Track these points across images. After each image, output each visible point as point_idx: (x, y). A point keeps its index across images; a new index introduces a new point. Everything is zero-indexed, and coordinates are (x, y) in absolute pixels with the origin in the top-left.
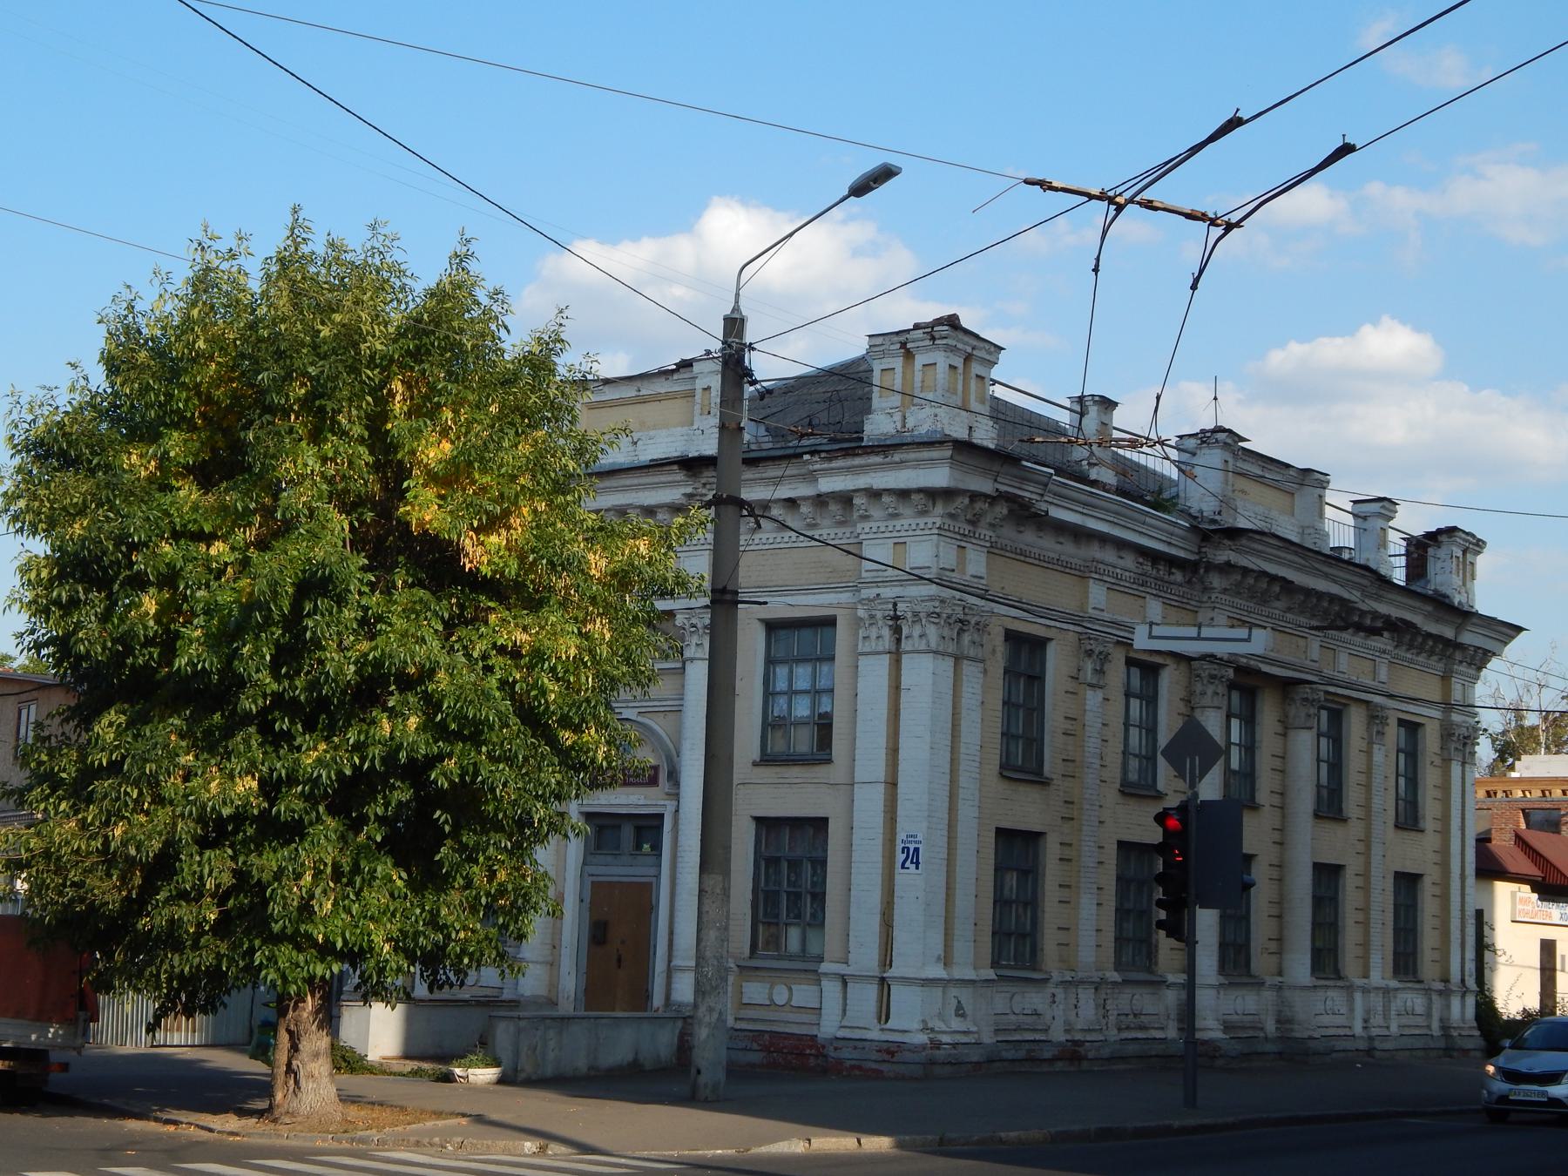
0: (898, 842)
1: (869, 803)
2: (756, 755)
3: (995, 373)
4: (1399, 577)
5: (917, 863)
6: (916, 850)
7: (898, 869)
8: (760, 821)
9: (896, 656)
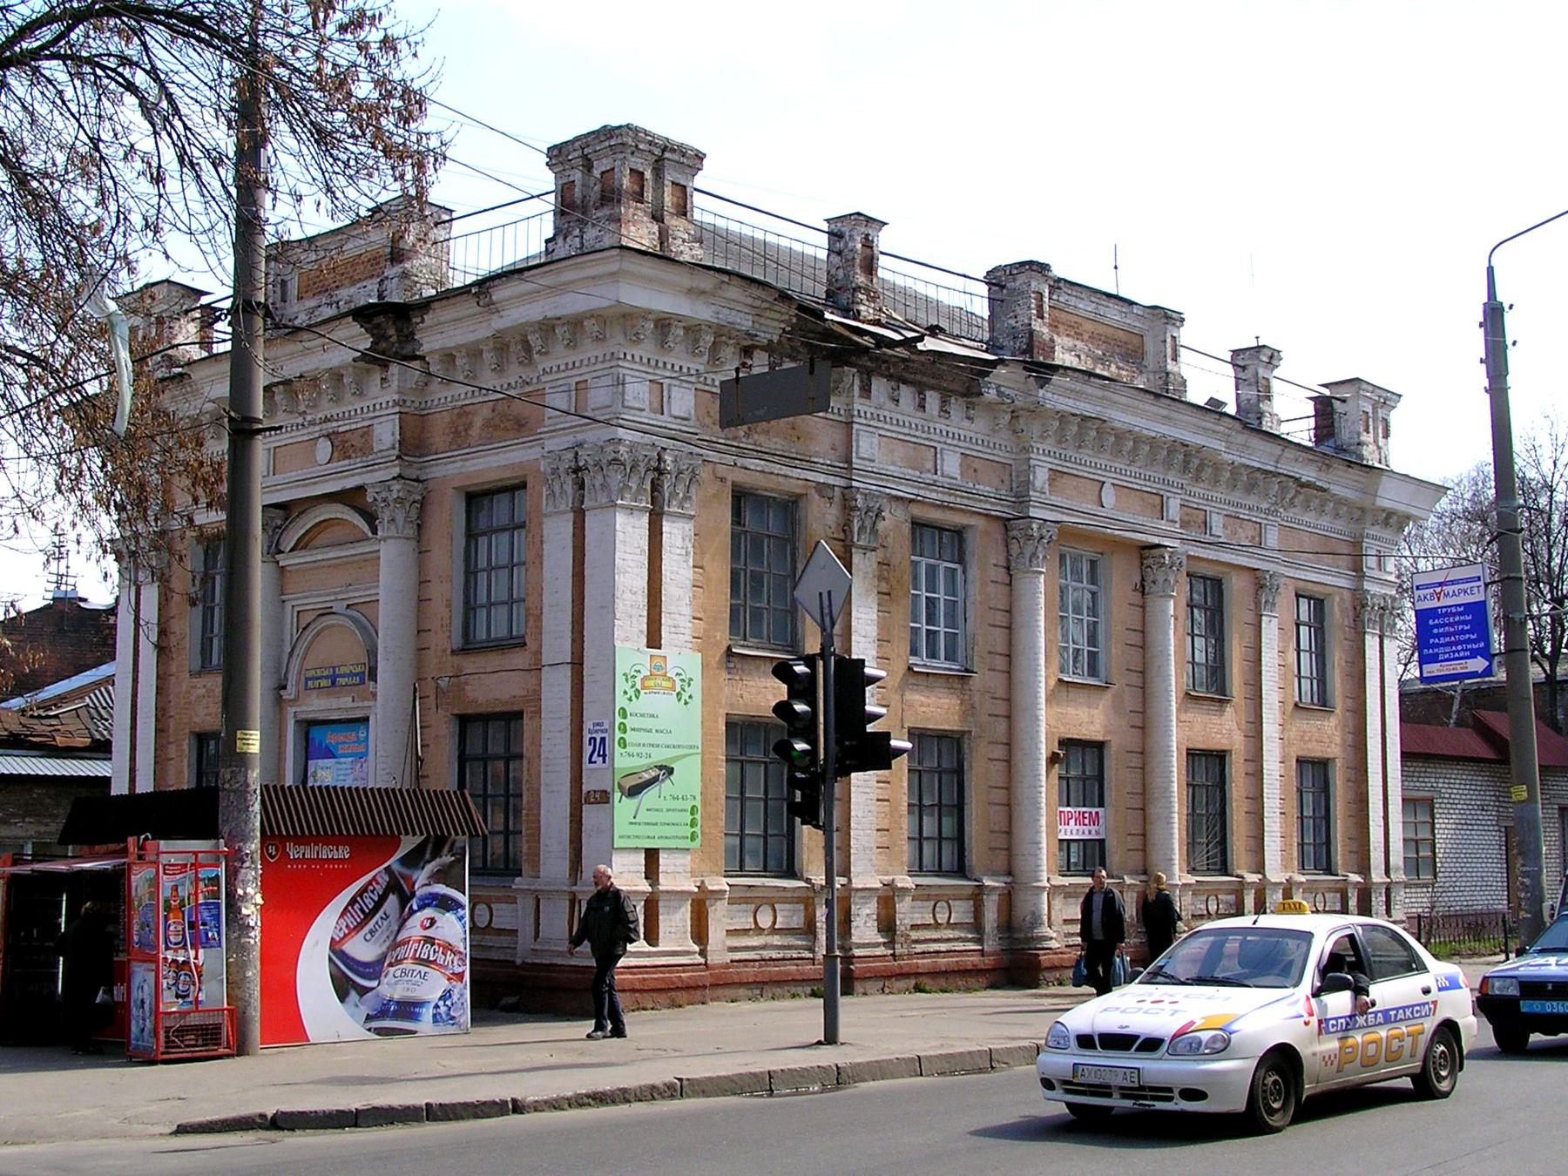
0: (585, 732)
1: (556, 690)
2: (457, 641)
4: (1302, 432)
5: (604, 756)
6: (603, 739)
7: (586, 765)
8: (464, 721)
9: (580, 515)
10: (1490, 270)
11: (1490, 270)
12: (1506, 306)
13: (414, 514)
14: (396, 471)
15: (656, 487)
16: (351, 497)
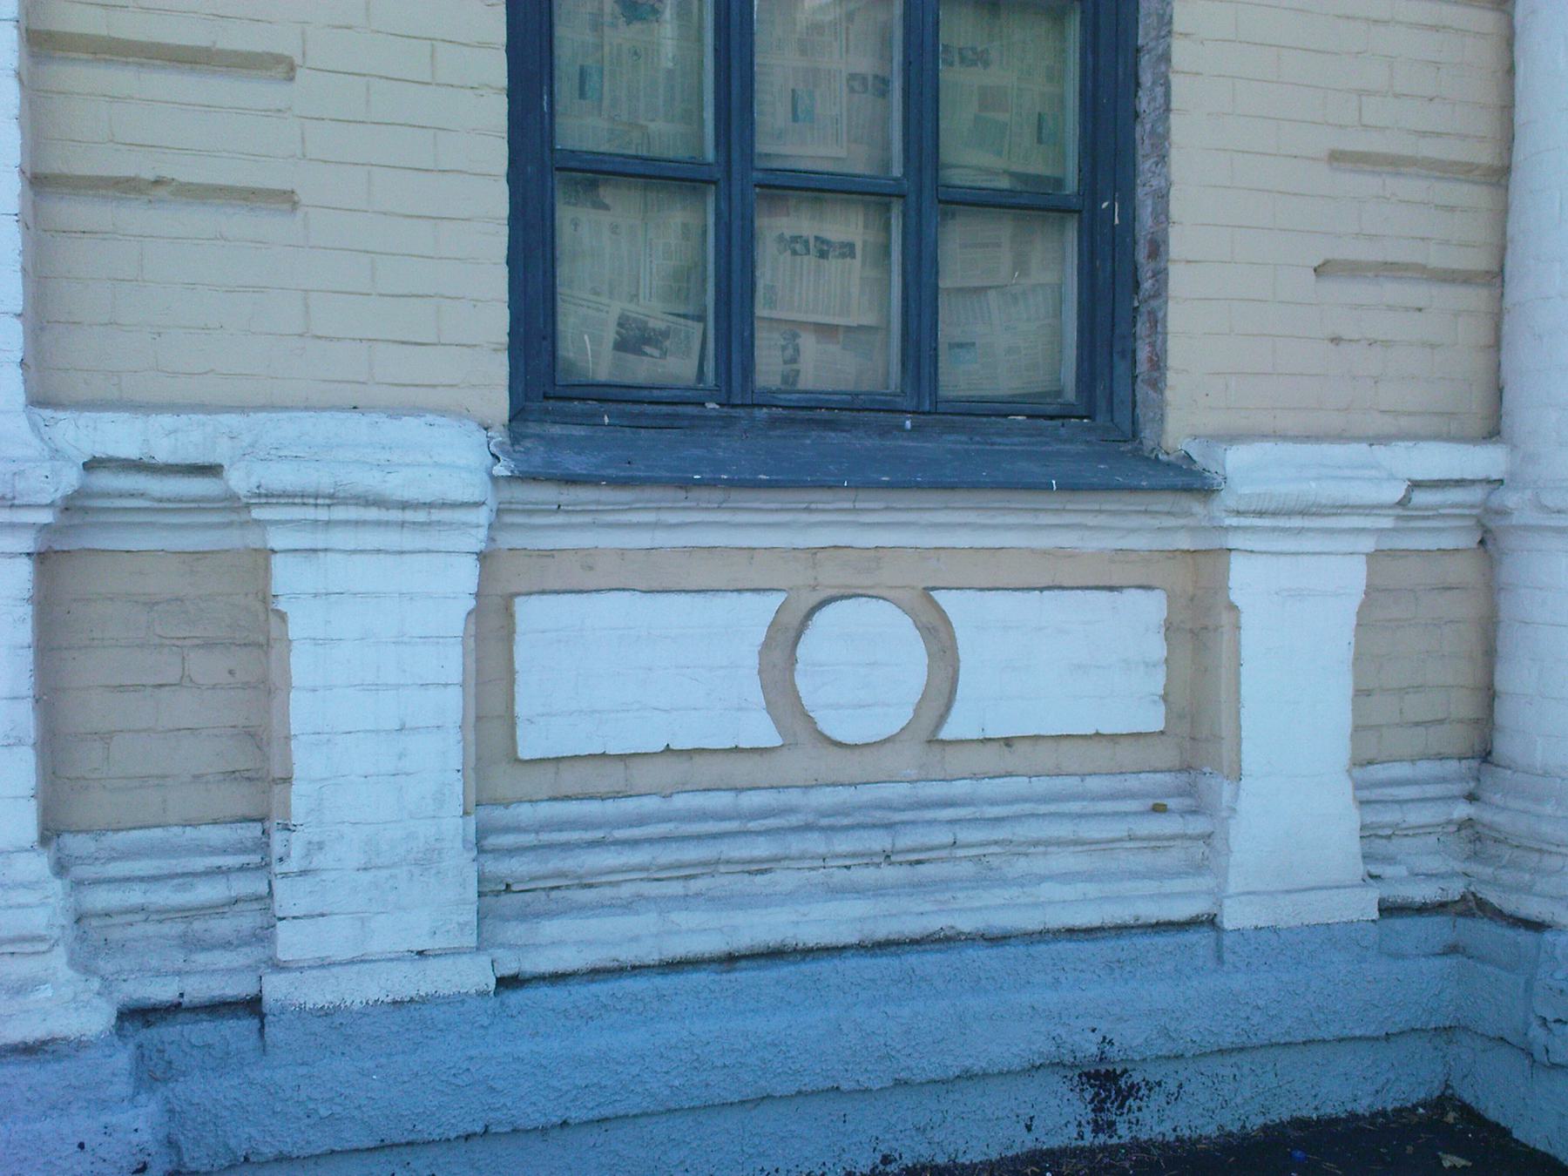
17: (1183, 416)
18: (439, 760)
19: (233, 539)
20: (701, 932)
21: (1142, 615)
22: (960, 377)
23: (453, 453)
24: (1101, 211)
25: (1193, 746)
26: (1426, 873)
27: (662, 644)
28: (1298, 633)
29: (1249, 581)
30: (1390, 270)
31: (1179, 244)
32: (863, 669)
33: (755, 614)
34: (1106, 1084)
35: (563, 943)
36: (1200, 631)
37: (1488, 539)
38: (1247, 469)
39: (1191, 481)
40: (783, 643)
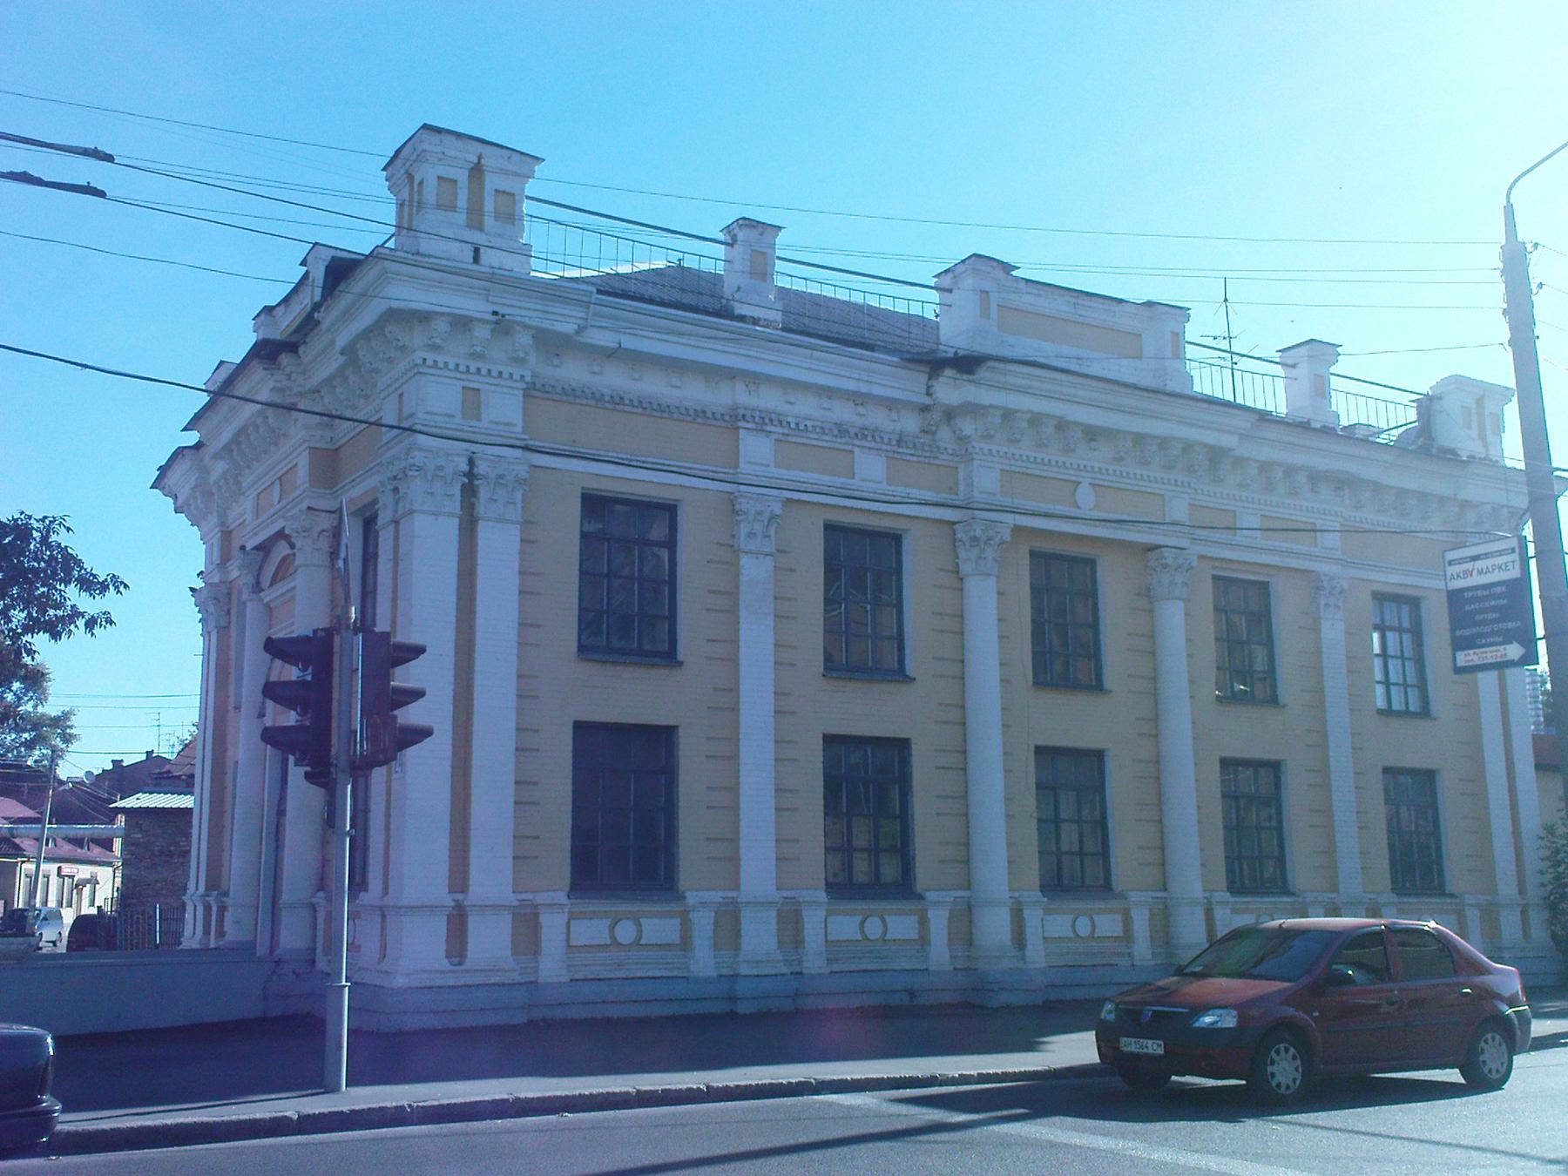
3: (531, 188)
10: (1509, 211)
11: (1509, 211)
12: (1529, 247)
13: (325, 544)
14: (304, 505)
15: (469, 491)
16: (281, 535)
17: (920, 885)
18: (821, 938)
19: (524, 896)
20: (854, 967)
21: (676, 921)
22: (883, 879)
23: (822, 896)
24: (904, 850)
25: (923, 940)
26: (961, 964)
27: (846, 926)
28: (939, 921)
29: (930, 914)
30: (723, 757)
31: (918, 858)
32: (874, 928)
33: (858, 919)
34: (912, 994)
35: (837, 967)
36: (923, 922)
37: (969, 908)
38: (931, 896)
39: (921, 897)
40: (612, 928)
